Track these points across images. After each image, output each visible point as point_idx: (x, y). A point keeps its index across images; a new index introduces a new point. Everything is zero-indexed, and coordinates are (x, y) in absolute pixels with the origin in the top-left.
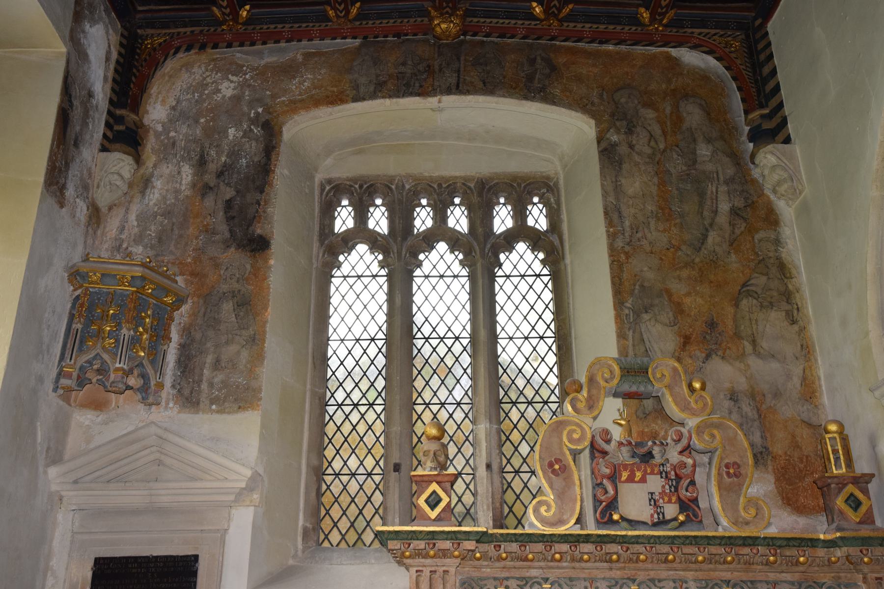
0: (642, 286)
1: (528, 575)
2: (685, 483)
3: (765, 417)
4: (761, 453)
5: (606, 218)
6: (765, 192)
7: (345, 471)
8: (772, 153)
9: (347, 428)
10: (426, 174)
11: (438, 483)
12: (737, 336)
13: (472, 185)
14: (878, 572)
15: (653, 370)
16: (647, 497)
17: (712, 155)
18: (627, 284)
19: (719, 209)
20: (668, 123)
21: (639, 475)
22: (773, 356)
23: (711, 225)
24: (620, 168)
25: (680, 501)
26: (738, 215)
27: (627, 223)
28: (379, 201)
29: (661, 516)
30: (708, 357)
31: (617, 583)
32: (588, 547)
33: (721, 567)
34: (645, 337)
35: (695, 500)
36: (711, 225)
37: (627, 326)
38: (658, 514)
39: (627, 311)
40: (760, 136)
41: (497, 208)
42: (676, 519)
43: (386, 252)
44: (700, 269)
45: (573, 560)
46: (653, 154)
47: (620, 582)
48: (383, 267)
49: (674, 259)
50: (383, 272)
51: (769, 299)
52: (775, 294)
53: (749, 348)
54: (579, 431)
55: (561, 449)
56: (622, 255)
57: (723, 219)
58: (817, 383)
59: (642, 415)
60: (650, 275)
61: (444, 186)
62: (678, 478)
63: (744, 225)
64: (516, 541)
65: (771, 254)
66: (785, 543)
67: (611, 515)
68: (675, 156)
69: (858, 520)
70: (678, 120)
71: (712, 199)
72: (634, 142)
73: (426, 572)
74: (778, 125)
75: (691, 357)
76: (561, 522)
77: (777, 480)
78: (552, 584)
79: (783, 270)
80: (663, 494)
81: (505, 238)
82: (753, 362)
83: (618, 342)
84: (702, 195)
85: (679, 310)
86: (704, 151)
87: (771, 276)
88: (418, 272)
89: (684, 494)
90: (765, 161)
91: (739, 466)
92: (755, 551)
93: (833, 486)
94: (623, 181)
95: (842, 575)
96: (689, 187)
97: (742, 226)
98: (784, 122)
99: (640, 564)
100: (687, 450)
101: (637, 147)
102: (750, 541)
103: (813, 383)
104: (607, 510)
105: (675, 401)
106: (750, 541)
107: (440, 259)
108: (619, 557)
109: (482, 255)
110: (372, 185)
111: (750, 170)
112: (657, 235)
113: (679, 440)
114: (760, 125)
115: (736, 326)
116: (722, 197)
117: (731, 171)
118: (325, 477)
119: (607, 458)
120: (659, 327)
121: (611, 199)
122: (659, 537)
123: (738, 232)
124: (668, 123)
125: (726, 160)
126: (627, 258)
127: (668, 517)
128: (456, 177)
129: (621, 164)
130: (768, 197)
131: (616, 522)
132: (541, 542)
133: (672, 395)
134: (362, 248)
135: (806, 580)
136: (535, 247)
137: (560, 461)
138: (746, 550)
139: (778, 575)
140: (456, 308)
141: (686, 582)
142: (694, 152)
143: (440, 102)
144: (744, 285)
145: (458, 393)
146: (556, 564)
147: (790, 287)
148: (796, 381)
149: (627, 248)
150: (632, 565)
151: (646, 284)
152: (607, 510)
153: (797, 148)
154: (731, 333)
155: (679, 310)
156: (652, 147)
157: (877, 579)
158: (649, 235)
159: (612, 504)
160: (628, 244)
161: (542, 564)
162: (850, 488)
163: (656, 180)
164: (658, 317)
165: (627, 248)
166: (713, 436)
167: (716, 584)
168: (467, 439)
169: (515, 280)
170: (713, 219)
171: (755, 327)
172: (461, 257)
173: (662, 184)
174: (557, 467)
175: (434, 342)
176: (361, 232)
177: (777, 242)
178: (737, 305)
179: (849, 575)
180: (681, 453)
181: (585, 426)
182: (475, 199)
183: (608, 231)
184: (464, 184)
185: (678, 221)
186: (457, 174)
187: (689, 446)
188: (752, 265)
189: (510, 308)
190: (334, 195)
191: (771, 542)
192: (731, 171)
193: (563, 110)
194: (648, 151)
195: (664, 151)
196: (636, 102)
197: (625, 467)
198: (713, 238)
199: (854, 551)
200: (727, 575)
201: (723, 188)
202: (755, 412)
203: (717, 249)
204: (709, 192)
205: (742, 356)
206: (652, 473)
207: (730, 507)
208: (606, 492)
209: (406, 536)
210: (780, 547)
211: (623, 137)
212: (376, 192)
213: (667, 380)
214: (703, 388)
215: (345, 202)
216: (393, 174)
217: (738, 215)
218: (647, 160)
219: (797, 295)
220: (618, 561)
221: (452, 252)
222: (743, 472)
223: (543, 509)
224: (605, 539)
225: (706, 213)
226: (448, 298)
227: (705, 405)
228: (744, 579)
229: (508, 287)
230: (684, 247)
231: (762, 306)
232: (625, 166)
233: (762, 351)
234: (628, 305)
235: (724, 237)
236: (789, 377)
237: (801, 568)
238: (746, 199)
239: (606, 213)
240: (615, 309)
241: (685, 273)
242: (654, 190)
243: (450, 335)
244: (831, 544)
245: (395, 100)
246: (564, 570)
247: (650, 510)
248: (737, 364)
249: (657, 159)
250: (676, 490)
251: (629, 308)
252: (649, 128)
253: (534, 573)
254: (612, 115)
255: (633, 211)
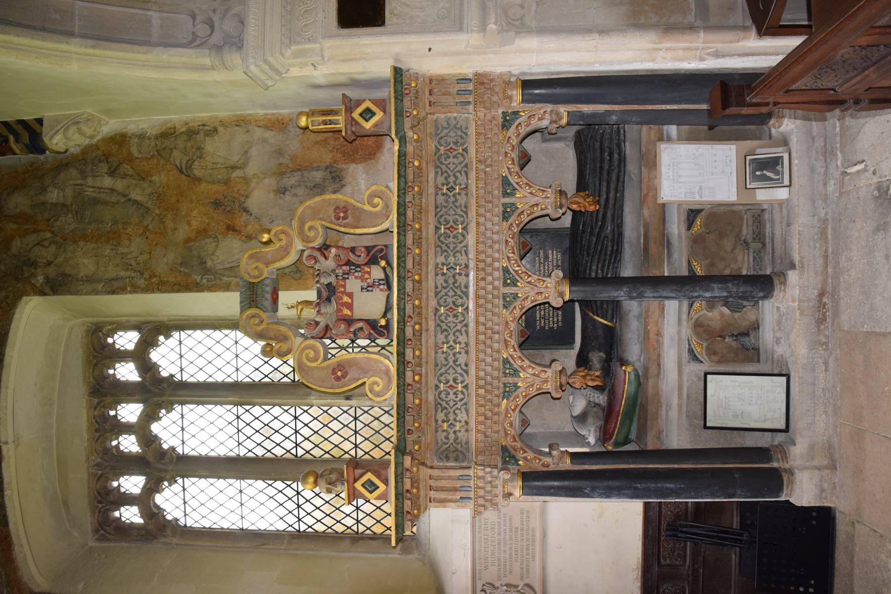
0: (181, 264)
1: (433, 403)
2: (353, 258)
3: (300, 165)
4: (331, 172)
5: (118, 293)
6: (94, 143)
7: (354, 515)
8: (51, 138)
9: (318, 514)
10: (86, 444)
11: (355, 480)
12: (227, 182)
13: (96, 401)
14: (425, 104)
15: (251, 277)
16: (365, 293)
17: (58, 188)
18: (179, 279)
19: (110, 187)
20: (26, 227)
21: (346, 299)
22: (246, 152)
23: (125, 196)
24: (70, 275)
25: (368, 264)
26: (115, 170)
27: (123, 273)
28: (115, 484)
29: (382, 282)
30: (246, 210)
31: (439, 325)
32: (409, 353)
33: (424, 234)
34: (228, 266)
35: (368, 249)
36: (125, 196)
37: (218, 281)
38: (380, 284)
39: (205, 281)
40: (36, 144)
41: (118, 376)
42: (384, 269)
43: (161, 480)
44: (166, 210)
45: (420, 365)
46: (56, 243)
47: (439, 322)
48: (176, 481)
49: (156, 233)
50: (180, 481)
51: (194, 150)
52: (189, 144)
53: (237, 173)
54: (307, 351)
55: (323, 368)
56: (153, 280)
57: (120, 185)
58: (270, 117)
59: (299, 275)
60: (171, 256)
61: (97, 426)
62: (348, 263)
63: (124, 165)
64: (404, 417)
65: (153, 144)
66: (403, 179)
67: (381, 326)
68: (58, 223)
69: (382, 113)
70: (23, 218)
71: (100, 193)
72: (45, 261)
73: (432, 494)
74: (25, 128)
75: (246, 226)
76: (387, 372)
77: (354, 161)
78: (440, 382)
79: (167, 134)
80: (363, 279)
81: (146, 373)
82: (251, 170)
83: (232, 291)
84: (96, 201)
85: (203, 232)
86: (53, 195)
87: (173, 146)
88: (179, 450)
89: (363, 258)
90: (61, 144)
91: (337, 208)
92: (410, 205)
93: (354, 129)
94: (82, 274)
95: (428, 131)
96: (88, 213)
97: (126, 168)
98: (22, 122)
99: (423, 304)
100: (324, 249)
101: (50, 258)
102: (402, 209)
103: (270, 120)
104: (375, 329)
105: (282, 258)
106: (402, 209)
107: (168, 429)
108: (416, 324)
109: (160, 392)
110: (98, 493)
111: (72, 154)
112: (134, 247)
113: (315, 258)
114: (26, 145)
115: (219, 182)
116: (98, 183)
117: (74, 173)
118: (360, 531)
119: (331, 326)
120: (219, 252)
121: (100, 286)
122: (399, 290)
123: (131, 172)
124: (26, 227)
125: (63, 175)
126: (156, 276)
127: (382, 276)
128: (88, 416)
129: (66, 275)
130: (99, 141)
131: (388, 321)
132: (404, 396)
133: (274, 262)
134: (159, 499)
135: (434, 161)
136: (154, 344)
137: (334, 369)
138: (409, 213)
139: (430, 184)
140: (211, 417)
141: (437, 264)
142: (55, 205)
143: (7, 443)
144: (181, 171)
145: (287, 418)
146: (423, 379)
147: (183, 129)
148: (268, 134)
149: (146, 275)
150: (424, 311)
151: (180, 261)
152: (375, 329)
153: (47, 114)
154: (225, 188)
155: (203, 232)
156: (50, 244)
157: (430, 105)
158: (134, 254)
159: (372, 323)
160: (142, 274)
161: (424, 390)
162: (356, 115)
163: (81, 244)
164: (210, 252)
165: (146, 275)
166: (311, 228)
167: (439, 238)
168: (326, 412)
169: (185, 363)
170: (119, 193)
171: (219, 166)
172: (163, 411)
173: (85, 238)
174: (339, 374)
175: (242, 438)
176: (144, 500)
177: (141, 137)
178: (199, 180)
179: (429, 125)
180: (326, 258)
181: (302, 346)
182: (109, 399)
183: (130, 292)
184: (95, 409)
185: (120, 227)
186: (85, 416)
187: (319, 249)
188: (162, 162)
189: (210, 369)
190: (109, 526)
191: (402, 191)
192: (74, 173)
193: (13, 326)
194: (53, 248)
195: (53, 233)
196: (5, 256)
197: (339, 310)
198: (136, 195)
199: (408, 123)
200: (432, 228)
201: (90, 181)
202: (296, 174)
203: (147, 192)
204: (94, 195)
205: (246, 180)
206: (344, 286)
207: (375, 218)
208: (361, 329)
209: (400, 518)
210: (406, 183)
211: (39, 271)
212: (105, 488)
213: (261, 265)
214: (269, 232)
215: (117, 514)
216: (86, 475)
217: (115, 170)
218: (62, 249)
219: (191, 124)
220: (420, 324)
221: (160, 419)
222: (342, 205)
223: (377, 389)
224: (401, 338)
225: (113, 199)
226: (202, 423)
227: (283, 232)
228: (433, 214)
229: (191, 369)
230: (145, 223)
231: (201, 157)
232: (68, 271)
233: (241, 161)
234: (199, 279)
235: (136, 185)
236: (264, 140)
237: (424, 165)
238: (100, 161)
239: (113, 292)
240: (202, 291)
241: (170, 224)
242: (91, 246)
243: (235, 423)
244: (403, 140)
245: (5, 486)
246: (428, 370)
247: (376, 291)
248: (252, 185)
249: (61, 241)
250: (359, 266)
251: (202, 278)
252: (31, 245)
253: (431, 398)
254: (18, 280)
255: (111, 267)
